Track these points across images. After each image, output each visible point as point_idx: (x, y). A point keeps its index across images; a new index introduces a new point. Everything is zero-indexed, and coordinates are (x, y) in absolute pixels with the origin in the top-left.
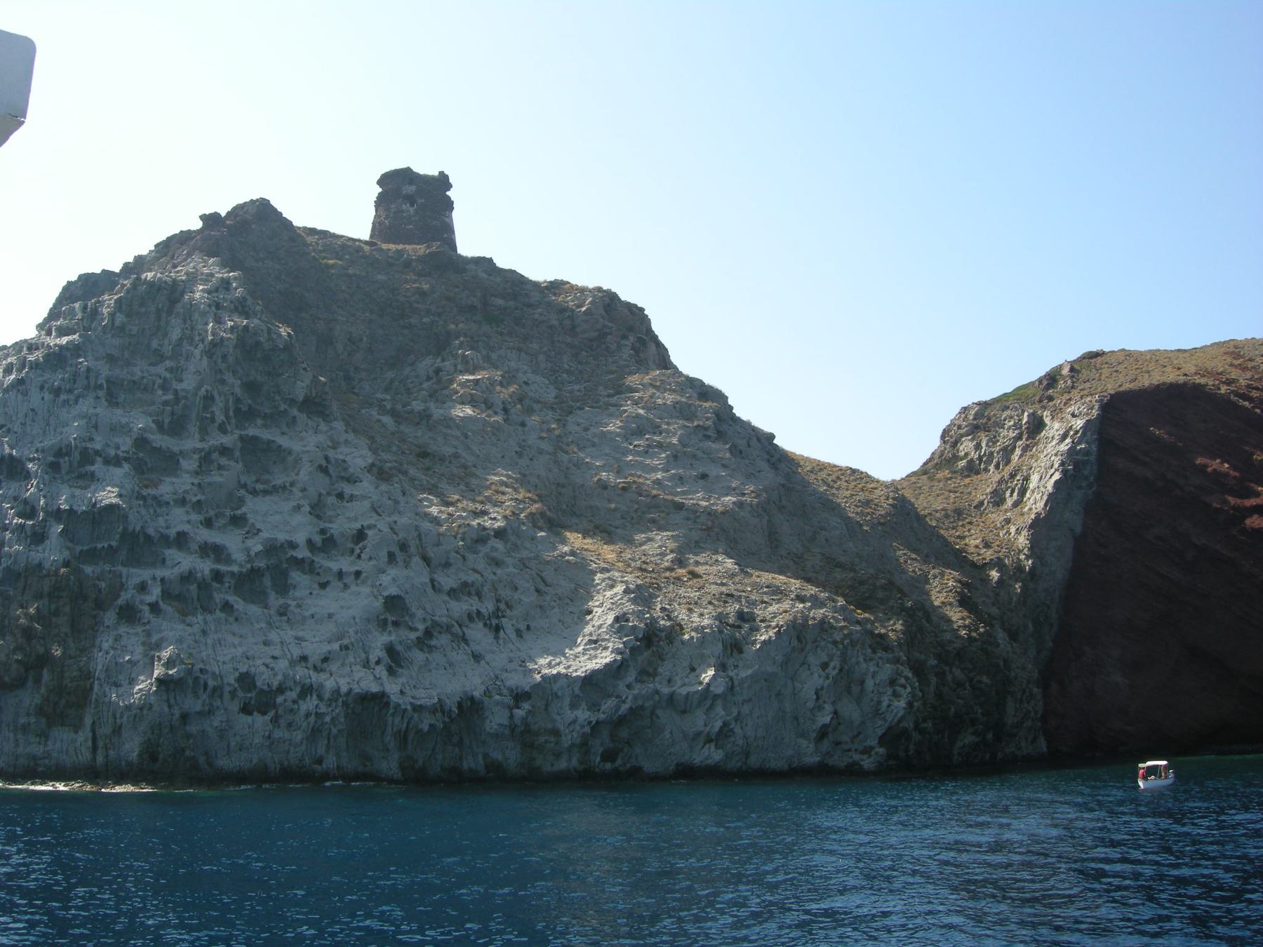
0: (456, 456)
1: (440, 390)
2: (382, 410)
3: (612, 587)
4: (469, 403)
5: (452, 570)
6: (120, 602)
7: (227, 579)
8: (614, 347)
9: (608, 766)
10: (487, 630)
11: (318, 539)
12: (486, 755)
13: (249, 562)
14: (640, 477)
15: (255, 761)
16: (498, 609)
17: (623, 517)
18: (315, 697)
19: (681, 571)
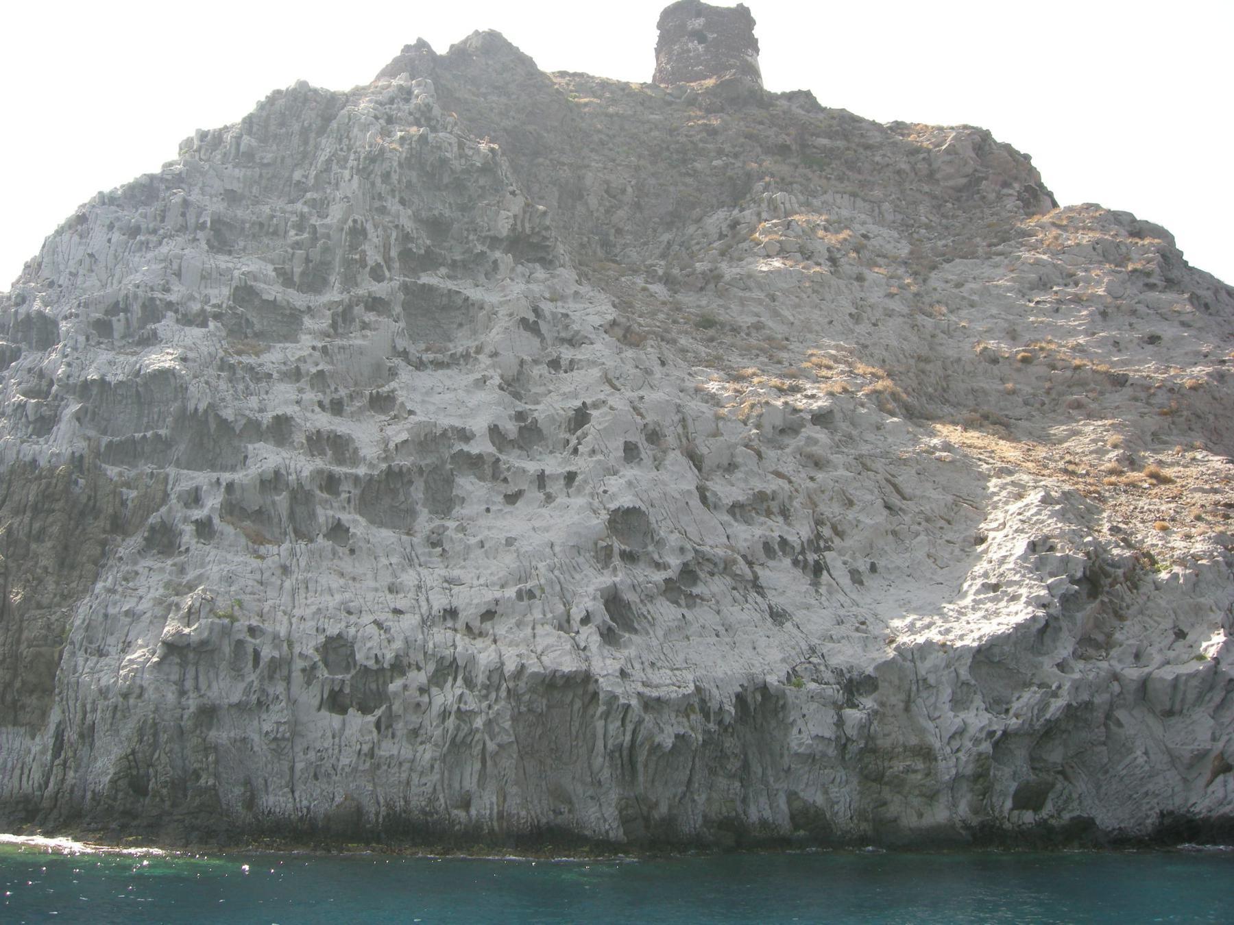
0: (758, 327)
1: (735, 240)
2: (651, 275)
3: (1020, 496)
4: (778, 254)
5: (739, 474)
6: (153, 519)
7: (345, 487)
8: (992, 196)
9: (1028, 817)
10: (798, 572)
11: (511, 428)
12: (792, 796)
13: (386, 459)
14: (1050, 342)
15: (338, 799)
16: (819, 536)
17: (1026, 403)
18: (460, 681)
19: (1135, 475)
